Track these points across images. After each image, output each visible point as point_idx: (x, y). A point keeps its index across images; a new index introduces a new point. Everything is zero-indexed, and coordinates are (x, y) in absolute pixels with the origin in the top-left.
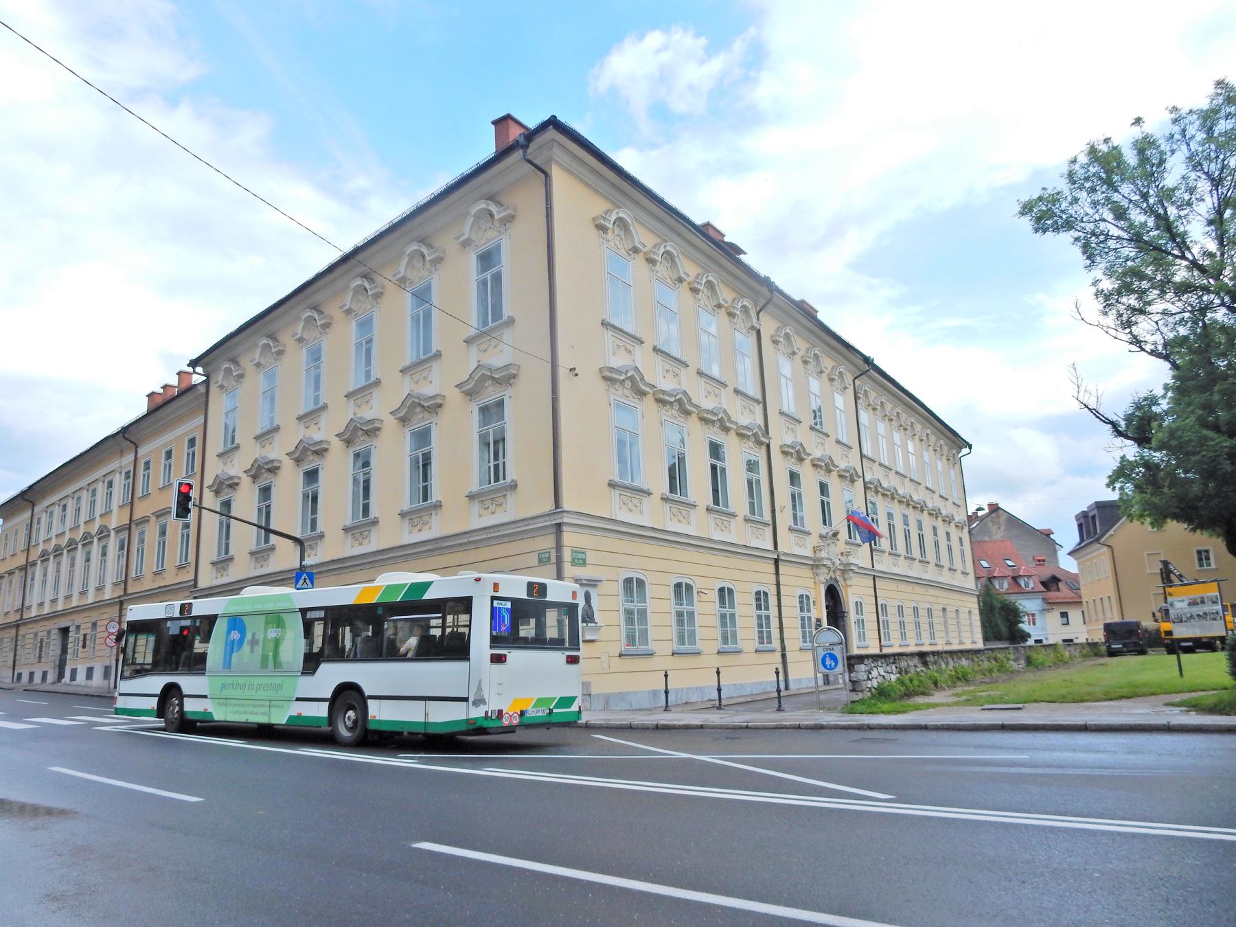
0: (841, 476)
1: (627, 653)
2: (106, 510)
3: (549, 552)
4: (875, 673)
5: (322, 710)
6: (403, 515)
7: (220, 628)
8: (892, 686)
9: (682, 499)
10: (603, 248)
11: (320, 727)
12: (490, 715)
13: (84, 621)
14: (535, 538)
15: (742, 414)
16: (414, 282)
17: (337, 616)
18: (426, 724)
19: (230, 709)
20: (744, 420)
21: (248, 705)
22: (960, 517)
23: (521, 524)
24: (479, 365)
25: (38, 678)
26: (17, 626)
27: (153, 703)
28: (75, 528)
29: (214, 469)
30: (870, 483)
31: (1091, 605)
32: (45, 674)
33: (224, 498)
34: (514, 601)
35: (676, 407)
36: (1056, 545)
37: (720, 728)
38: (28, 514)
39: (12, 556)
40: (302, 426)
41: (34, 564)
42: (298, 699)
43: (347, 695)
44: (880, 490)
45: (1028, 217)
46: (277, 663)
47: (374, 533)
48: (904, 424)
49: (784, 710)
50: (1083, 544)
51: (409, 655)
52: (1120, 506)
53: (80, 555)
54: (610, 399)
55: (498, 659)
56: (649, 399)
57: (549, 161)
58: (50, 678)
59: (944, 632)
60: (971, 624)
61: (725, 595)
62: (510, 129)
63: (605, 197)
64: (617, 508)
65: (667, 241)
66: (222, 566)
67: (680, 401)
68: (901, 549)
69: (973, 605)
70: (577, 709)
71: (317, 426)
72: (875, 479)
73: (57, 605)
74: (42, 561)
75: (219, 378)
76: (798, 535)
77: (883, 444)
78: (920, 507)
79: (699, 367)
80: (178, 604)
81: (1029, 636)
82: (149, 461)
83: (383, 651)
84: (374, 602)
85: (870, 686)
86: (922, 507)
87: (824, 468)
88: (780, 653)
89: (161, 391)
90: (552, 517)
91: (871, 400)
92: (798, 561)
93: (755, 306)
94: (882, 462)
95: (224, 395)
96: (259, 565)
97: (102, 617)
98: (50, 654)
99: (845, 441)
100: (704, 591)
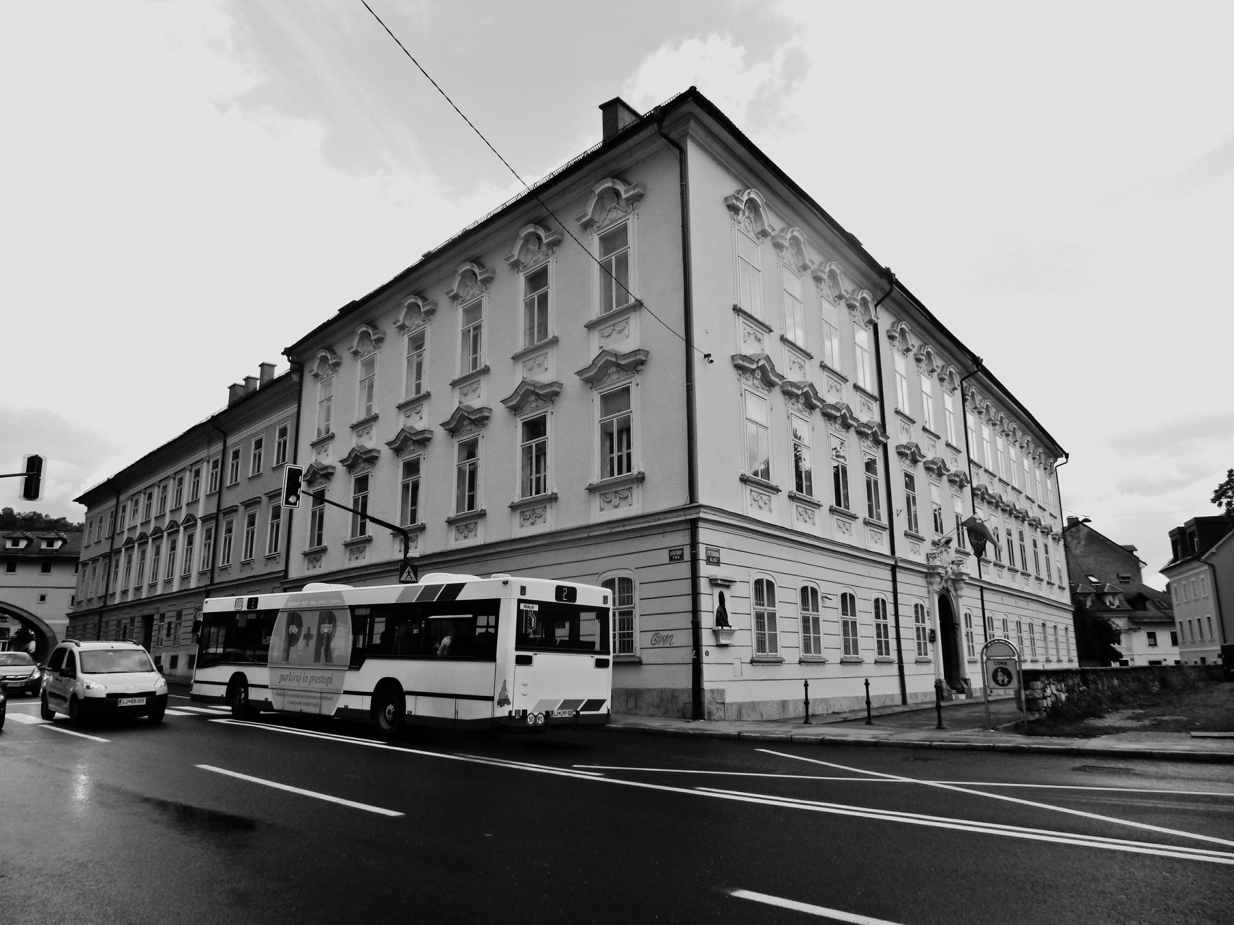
0: (951, 481)
2: (192, 499)
3: (682, 550)
4: (1048, 691)
6: (514, 507)
9: (808, 498)
12: (513, 714)
14: (666, 534)
15: (861, 411)
16: (529, 266)
19: (287, 699)
22: (1057, 529)
23: (641, 521)
26: (101, 612)
28: (147, 523)
29: (306, 459)
30: (978, 489)
31: (1186, 626)
38: (113, 502)
39: (96, 543)
41: (119, 551)
42: (346, 692)
43: (389, 690)
44: (987, 497)
47: (481, 527)
48: (1006, 430)
49: (944, 728)
50: (1177, 563)
55: (523, 661)
56: (777, 391)
57: (685, 135)
59: (1044, 649)
61: (848, 602)
62: (619, 114)
64: (744, 503)
66: (315, 558)
67: (806, 395)
69: (1067, 620)
71: (419, 415)
73: (142, 593)
77: (987, 448)
79: (822, 359)
80: (246, 598)
81: (1121, 656)
83: (423, 650)
84: (414, 601)
85: (1045, 705)
87: (936, 472)
89: (243, 383)
90: (687, 512)
92: (913, 568)
94: (987, 468)
95: (319, 385)
96: (354, 557)
100: (829, 596)
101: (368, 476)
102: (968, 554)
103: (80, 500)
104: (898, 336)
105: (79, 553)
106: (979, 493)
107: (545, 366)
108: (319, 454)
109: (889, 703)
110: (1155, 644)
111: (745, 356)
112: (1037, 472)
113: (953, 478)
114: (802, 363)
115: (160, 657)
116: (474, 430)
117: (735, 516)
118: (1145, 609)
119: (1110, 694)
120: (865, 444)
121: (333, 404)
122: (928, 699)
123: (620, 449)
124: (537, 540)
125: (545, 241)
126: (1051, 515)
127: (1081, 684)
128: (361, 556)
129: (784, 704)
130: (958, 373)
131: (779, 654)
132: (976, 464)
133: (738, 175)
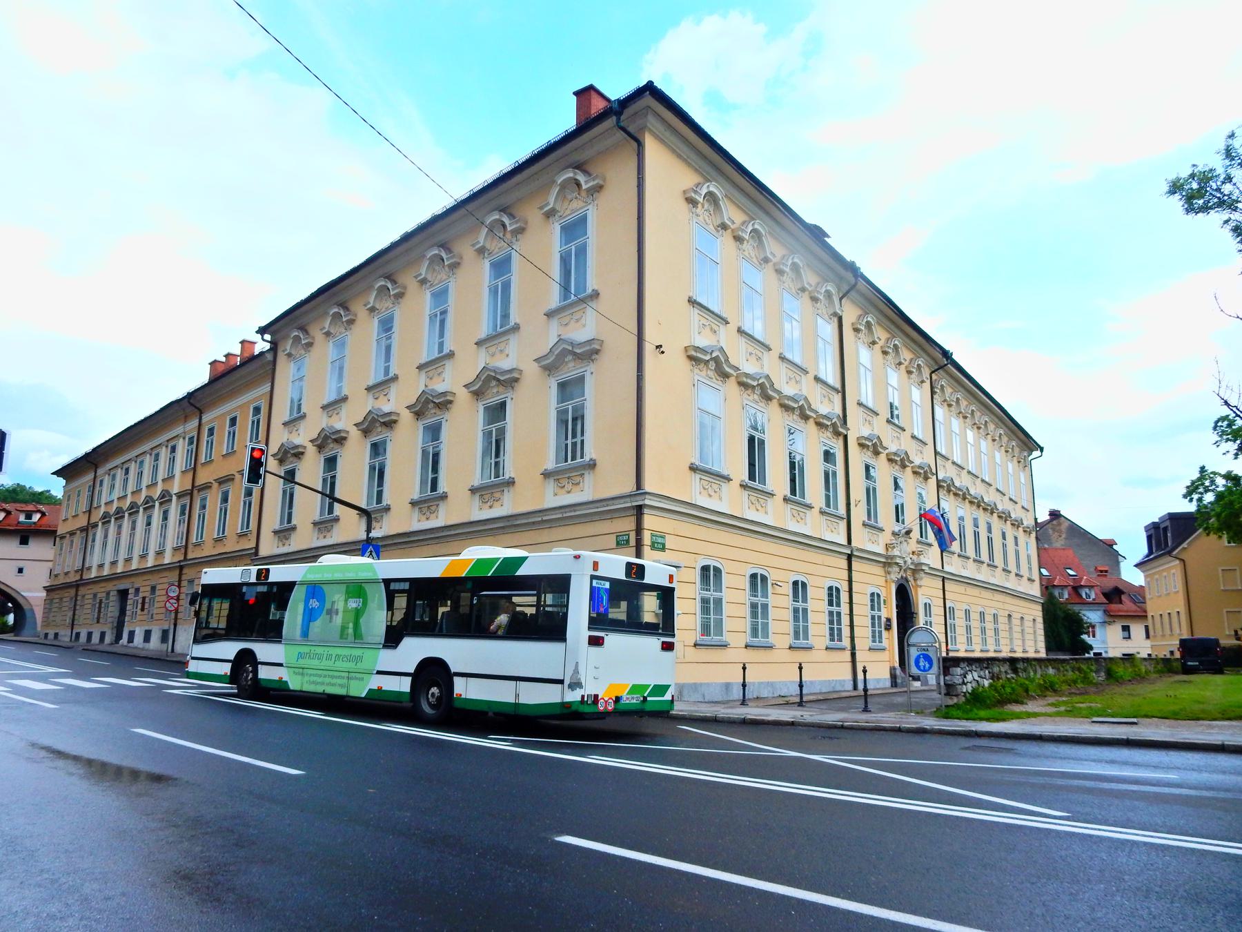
0: (915, 473)
1: (703, 643)
3: (628, 535)
4: (969, 677)
5: (404, 685)
6: (473, 491)
7: (297, 596)
8: (986, 691)
9: (760, 487)
10: (693, 221)
11: (401, 702)
12: (586, 699)
13: (144, 585)
16: (494, 253)
17: (423, 590)
18: (516, 705)
19: (306, 678)
20: (824, 409)
21: (325, 676)
22: (1028, 522)
23: (591, 506)
24: (560, 339)
25: (96, 638)
26: (77, 586)
27: (226, 669)
29: (279, 437)
30: (944, 481)
31: (1157, 619)
32: (103, 635)
33: (289, 467)
34: (614, 582)
35: (758, 391)
36: (1120, 557)
37: (813, 727)
39: (73, 517)
40: (325, 415)
41: (95, 526)
42: (379, 673)
44: (953, 489)
45: (1177, 196)
46: (357, 634)
47: (443, 508)
48: (978, 423)
49: (870, 711)
50: (1151, 557)
51: (500, 633)
52: (1197, 518)
53: (141, 519)
54: (694, 379)
55: (595, 642)
56: (732, 382)
57: (643, 129)
58: (108, 639)
59: (1008, 640)
60: (1035, 632)
61: (799, 589)
63: (696, 170)
64: (695, 492)
65: (754, 219)
67: (762, 386)
68: (970, 551)
69: (1037, 612)
70: (670, 699)
72: (948, 477)
74: (103, 523)
75: (287, 346)
76: (871, 531)
78: (990, 509)
79: (781, 351)
80: (254, 569)
81: (1091, 648)
82: (214, 427)
84: (463, 575)
85: (965, 691)
86: (992, 509)
87: (899, 463)
88: (850, 652)
89: (224, 359)
91: (947, 395)
92: (870, 557)
93: (838, 293)
96: (322, 536)
97: (162, 582)
98: (109, 615)
99: (920, 437)
100: (779, 583)
101: (386, 440)
102: (930, 545)
103: (58, 473)
104: (863, 329)
105: (56, 526)
106: (945, 485)
107: (507, 352)
108: (291, 433)
109: (838, 688)
110: (1129, 638)
111: (698, 347)
112: (1010, 465)
113: (918, 470)
114: (760, 355)
115: (134, 631)
116: (437, 414)
117: (681, 504)
118: (1121, 602)
119: (1042, 683)
120: (825, 436)
121: (304, 384)
122: (881, 685)
123: (574, 436)
124: (495, 523)
125: (509, 229)
126: (1023, 507)
127: (1009, 671)
128: (328, 535)
129: (727, 686)
130: (928, 366)
131: (724, 638)
132: (943, 456)
133: (698, 168)
